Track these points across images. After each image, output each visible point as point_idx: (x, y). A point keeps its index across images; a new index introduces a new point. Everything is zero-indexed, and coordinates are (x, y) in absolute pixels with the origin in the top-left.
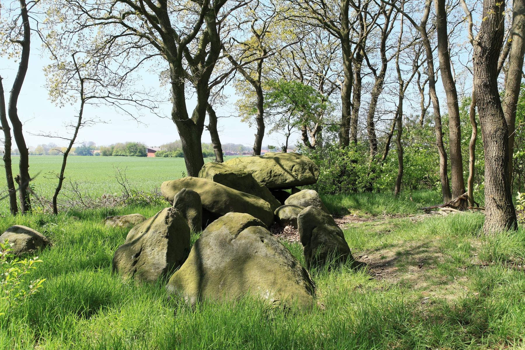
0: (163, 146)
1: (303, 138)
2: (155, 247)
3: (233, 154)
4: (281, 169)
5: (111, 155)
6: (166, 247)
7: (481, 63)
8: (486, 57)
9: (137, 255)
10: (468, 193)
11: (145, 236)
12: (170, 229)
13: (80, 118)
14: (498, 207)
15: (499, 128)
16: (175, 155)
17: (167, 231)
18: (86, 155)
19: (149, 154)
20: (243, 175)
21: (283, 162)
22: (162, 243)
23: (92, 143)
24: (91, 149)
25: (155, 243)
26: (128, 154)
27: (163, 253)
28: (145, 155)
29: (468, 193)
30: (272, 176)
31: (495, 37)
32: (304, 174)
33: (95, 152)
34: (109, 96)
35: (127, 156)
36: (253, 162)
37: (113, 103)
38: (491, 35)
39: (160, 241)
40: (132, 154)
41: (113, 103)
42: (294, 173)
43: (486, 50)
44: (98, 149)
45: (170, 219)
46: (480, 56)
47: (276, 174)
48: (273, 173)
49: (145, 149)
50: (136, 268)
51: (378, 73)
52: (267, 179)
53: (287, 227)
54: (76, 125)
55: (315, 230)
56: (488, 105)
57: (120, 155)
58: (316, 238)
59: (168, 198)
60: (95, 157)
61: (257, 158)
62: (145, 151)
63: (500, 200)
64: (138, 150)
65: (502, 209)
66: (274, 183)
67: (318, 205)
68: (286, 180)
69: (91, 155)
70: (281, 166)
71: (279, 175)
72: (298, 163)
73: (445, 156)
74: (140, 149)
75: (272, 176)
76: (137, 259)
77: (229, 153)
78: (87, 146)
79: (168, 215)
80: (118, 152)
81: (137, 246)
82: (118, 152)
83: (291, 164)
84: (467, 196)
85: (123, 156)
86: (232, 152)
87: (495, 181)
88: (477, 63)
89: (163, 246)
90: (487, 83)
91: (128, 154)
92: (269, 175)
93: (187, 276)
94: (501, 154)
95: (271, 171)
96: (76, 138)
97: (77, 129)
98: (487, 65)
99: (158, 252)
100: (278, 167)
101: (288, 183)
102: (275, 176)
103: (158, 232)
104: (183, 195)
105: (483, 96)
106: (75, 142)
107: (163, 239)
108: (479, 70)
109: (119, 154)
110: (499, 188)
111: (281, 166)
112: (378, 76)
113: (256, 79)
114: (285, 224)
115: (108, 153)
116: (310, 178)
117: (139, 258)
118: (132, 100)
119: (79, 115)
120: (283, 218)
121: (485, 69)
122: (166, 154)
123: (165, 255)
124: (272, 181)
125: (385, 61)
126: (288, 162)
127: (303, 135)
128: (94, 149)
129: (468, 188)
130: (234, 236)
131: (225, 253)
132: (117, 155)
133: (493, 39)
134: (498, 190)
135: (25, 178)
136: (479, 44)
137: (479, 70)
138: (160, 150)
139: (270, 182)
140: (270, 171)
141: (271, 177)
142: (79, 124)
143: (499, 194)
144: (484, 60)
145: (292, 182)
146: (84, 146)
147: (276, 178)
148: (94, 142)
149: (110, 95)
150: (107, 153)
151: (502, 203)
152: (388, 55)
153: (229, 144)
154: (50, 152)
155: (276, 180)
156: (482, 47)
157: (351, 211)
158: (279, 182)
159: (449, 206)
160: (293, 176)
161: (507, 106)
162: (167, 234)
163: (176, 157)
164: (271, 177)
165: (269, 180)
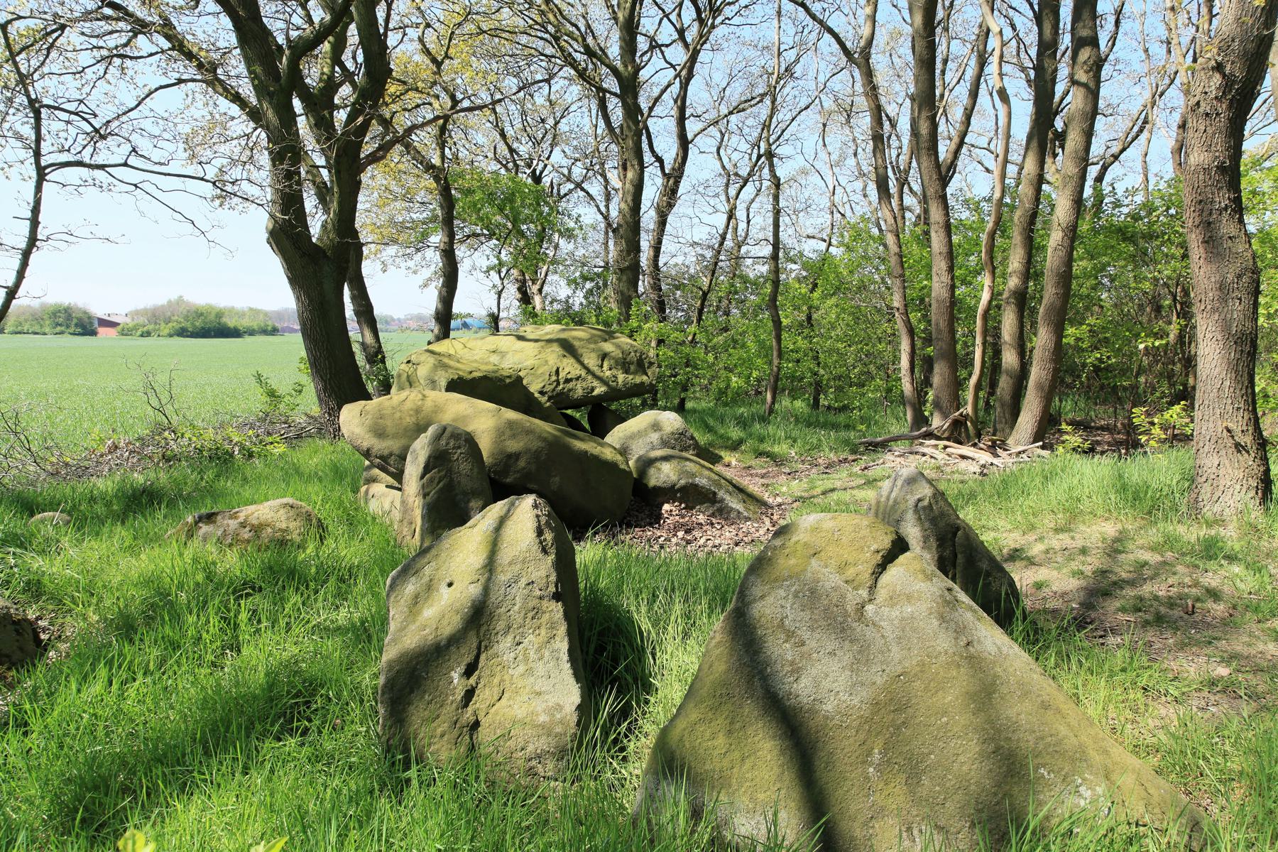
0: (137, 313)
1: (519, 296)
2: (523, 635)
6: (562, 629)
7: (1217, 114)
8: (1231, 100)
13: (35, 223)
15: (1246, 269)
16: (166, 331)
17: (553, 578)
19: (101, 330)
20: (508, 381)
22: (546, 617)
25: (520, 621)
26: (47, 330)
27: (558, 651)
28: (93, 333)
30: (562, 381)
31: (1257, 53)
34: (129, 162)
35: (45, 334)
37: (136, 185)
38: (1249, 46)
39: (537, 612)
40: (59, 329)
41: (136, 185)
43: (1234, 82)
45: (549, 536)
46: (1216, 98)
47: (569, 377)
48: (562, 375)
49: (90, 318)
50: (475, 713)
52: (548, 388)
53: (666, 507)
54: (23, 245)
56: (1220, 214)
59: (368, 450)
62: (91, 324)
63: (1243, 431)
64: (75, 321)
65: (1248, 452)
66: (568, 396)
67: (689, 447)
71: (577, 379)
74: (80, 319)
75: (562, 381)
76: (472, 681)
79: (539, 521)
84: (967, 416)
87: (1232, 390)
88: (1207, 115)
89: (552, 626)
90: (1225, 162)
92: (554, 378)
95: (558, 369)
96: (24, 281)
97: (26, 255)
98: (1230, 120)
99: (539, 649)
102: (567, 381)
103: (523, 582)
104: (443, 442)
105: (1213, 194)
106: (21, 292)
107: (545, 603)
108: (1210, 131)
110: (1242, 405)
112: (667, 171)
114: (660, 500)
117: (479, 678)
118: (202, 179)
119: (29, 215)
120: (659, 484)
121: (1224, 129)
122: (145, 329)
123: (565, 657)
124: (561, 393)
125: (684, 143)
127: (519, 289)
130: (864, 593)
131: (859, 652)
133: (1252, 55)
134: (1238, 409)
136: (1219, 67)
137: (1210, 131)
138: (128, 320)
139: (558, 394)
140: (555, 369)
141: (558, 382)
142: (33, 240)
143: (1240, 419)
144: (1224, 106)
147: (570, 385)
149: (133, 161)
152: (692, 127)
155: (570, 390)
156: (1224, 75)
157: (722, 454)
161: (1063, 231)
162: (556, 586)
163: (171, 336)
164: (558, 382)
165: (554, 390)
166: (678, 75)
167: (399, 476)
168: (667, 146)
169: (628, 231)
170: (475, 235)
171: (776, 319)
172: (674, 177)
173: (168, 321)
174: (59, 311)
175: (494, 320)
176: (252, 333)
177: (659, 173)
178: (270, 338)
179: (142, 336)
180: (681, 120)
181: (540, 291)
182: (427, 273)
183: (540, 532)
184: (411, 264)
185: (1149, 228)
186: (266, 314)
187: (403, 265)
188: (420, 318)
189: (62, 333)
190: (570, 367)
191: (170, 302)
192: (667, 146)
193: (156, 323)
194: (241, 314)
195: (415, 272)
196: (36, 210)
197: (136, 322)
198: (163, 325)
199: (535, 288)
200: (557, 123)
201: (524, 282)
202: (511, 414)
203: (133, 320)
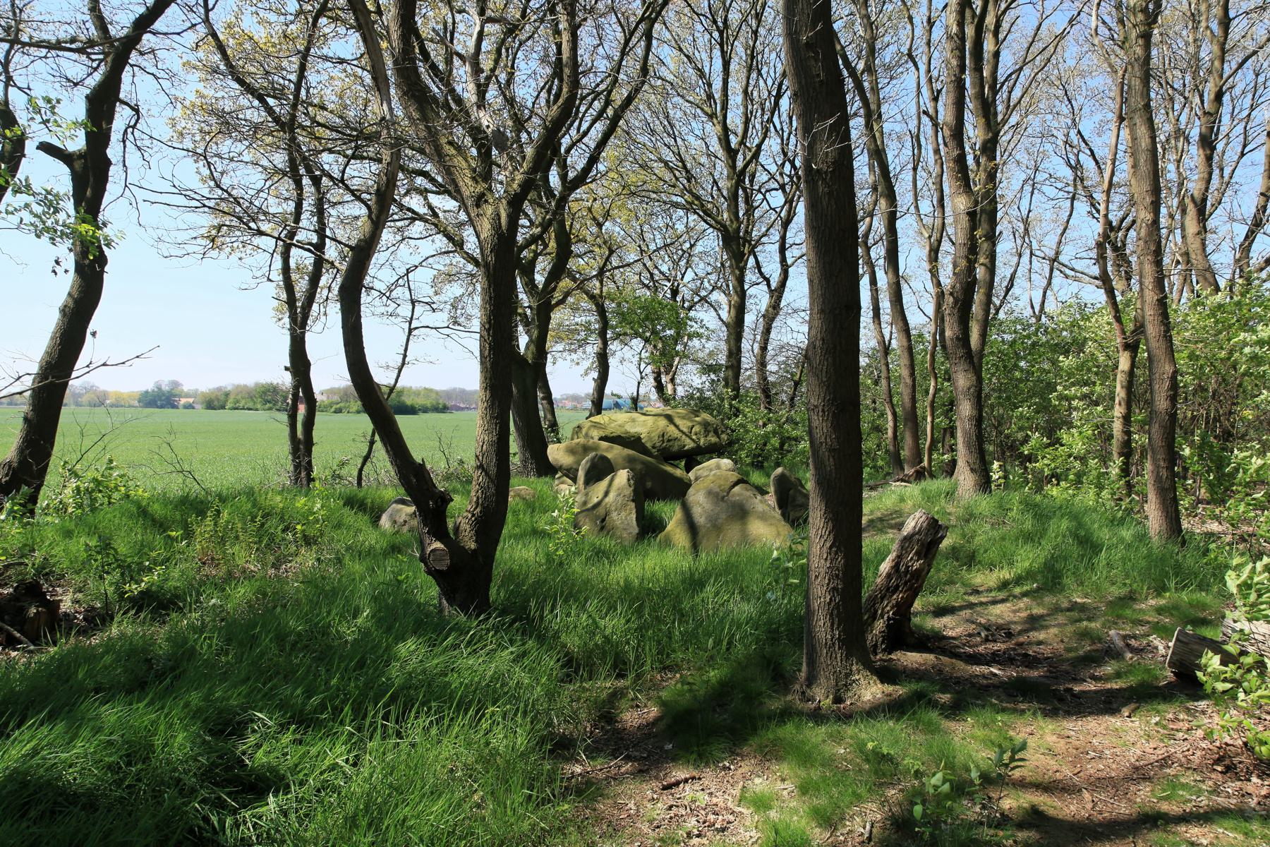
3: (462, 409)
4: (676, 432)
5: (223, 407)
6: (634, 511)
9: (603, 520)
10: (925, 463)
11: (607, 500)
12: (634, 491)
13: (405, 356)
14: (972, 470)
18: (162, 407)
21: (678, 421)
23: (175, 384)
24: (175, 396)
26: (259, 406)
29: (925, 463)
32: (708, 438)
33: (183, 401)
35: (257, 410)
36: (633, 420)
39: (626, 505)
40: (268, 405)
42: (694, 437)
44: (188, 396)
45: (632, 482)
51: (774, 285)
52: (658, 445)
55: (791, 492)
57: (243, 409)
58: (794, 500)
60: (181, 410)
61: (635, 415)
68: (684, 446)
69: (174, 407)
70: (677, 427)
72: (699, 423)
73: (894, 414)
77: (455, 406)
78: (165, 388)
80: (238, 402)
81: (601, 511)
82: (238, 402)
83: (690, 424)
84: (924, 468)
85: (250, 409)
86: (462, 405)
89: (631, 510)
91: (259, 406)
93: (677, 536)
94: (975, 413)
100: (672, 428)
101: (688, 450)
109: (241, 405)
111: (677, 427)
113: (597, 292)
115: (216, 403)
116: (716, 443)
124: (664, 449)
126: (685, 421)
128: (180, 396)
129: (926, 458)
132: (236, 409)
135: (309, 442)
142: (403, 364)
145: (693, 449)
146: (159, 389)
147: (671, 443)
148: (181, 381)
150: (215, 402)
151: (977, 466)
153: (454, 390)
154: (84, 399)
158: (675, 448)
159: (902, 480)
160: (693, 440)
167: (574, 480)
170: (625, 334)
172: (777, 293)
174: (269, 391)
175: (635, 400)
176: (425, 410)
177: (766, 288)
178: (442, 416)
179: (335, 412)
180: (783, 250)
181: (672, 380)
182: (586, 364)
183: (629, 480)
184: (574, 356)
186: (437, 393)
187: (568, 358)
188: (575, 398)
189: (270, 409)
194: (417, 393)
195: (578, 364)
196: (406, 350)
200: (692, 246)
202: (631, 452)
203: (328, 398)
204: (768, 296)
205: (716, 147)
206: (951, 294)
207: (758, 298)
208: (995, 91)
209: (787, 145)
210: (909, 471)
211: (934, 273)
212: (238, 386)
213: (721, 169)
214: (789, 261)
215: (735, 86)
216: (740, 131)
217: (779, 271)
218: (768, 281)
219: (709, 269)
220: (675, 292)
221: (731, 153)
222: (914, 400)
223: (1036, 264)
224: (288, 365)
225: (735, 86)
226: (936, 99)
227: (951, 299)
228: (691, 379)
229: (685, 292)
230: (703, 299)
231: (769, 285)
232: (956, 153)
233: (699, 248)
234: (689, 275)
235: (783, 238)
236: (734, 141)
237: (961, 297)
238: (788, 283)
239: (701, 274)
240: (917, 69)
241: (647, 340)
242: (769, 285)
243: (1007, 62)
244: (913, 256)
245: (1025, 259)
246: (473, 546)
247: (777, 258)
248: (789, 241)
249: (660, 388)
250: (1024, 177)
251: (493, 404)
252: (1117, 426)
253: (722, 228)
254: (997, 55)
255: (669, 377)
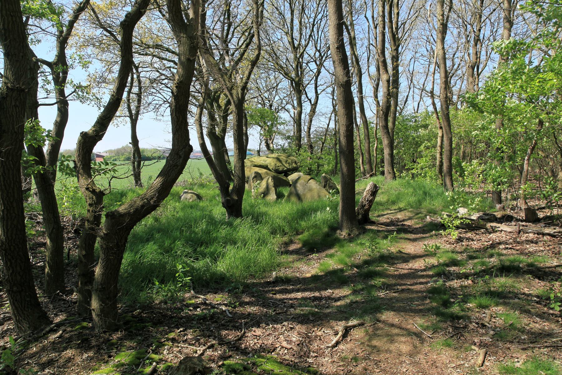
1: (265, 144)
16: (122, 159)
29: (374, 172)
48: (277, 165)
102: (278, 166)
124: (277, 169)
138: (108, 154)
166: (315, 75)
168: (311, 94)
169: (298, 121)
171: (213, 285)
172: (314, 106)
173: (123, 155)
175: (259, 152)
177: (310, 104)
180: (316, 87)
181: (272, 142)
185: (68, 265)
190: (279, 164)
191: (123, 147)
192: (311, 94)
193: (118, 156)
194: (150, 151)
197: (111, 155)
198: (121, 156)
199: (271, 142)
201: (267, 140)
204: (310, 107)
205: (288, 45)
206: (382, 110)
207: (307, 108)
208: (397, 29)
209: (317, 44)
210: (368, 176)
211: (376, 97)
212: (66, 150)
213: (291, 56)
214: (319, 92)
215: (296, 22)
216: (298, 38)
217: (315, 97)
218: (310, 100)
219: (285, 95)
220: (271, 106)
221: (295, 49)
222: (260, 42)
223: (416, 90)
224: (131, 142)
225: (296, 22)
226: (376, 28)
227: (382, 112)
228: (279, 142)
229: (275, 105)
230: (283, 108)
231: (311, 102)
232: (383, 59)
233: (279, 87)
234: (277, 98)
235: (316, 84)
236: (296, 43)
237: (385, 111)
238: (319, 102)
239: (282, 97)
240: (368, 22)
241: (261, 127)
242: (311, 102)
243: (403, 16)
244: (368, 89)
245: (412, 89)
246: (237, 198)
247: (314, 91)
248: (319, 83)
249: (268, 146)
250: (411, 56)
251: (239, 154)
252: (438, 156)
253: (292, 80)
254: (398, 14)
255: (271, 141)
